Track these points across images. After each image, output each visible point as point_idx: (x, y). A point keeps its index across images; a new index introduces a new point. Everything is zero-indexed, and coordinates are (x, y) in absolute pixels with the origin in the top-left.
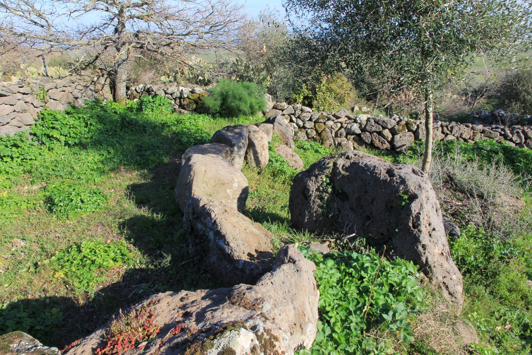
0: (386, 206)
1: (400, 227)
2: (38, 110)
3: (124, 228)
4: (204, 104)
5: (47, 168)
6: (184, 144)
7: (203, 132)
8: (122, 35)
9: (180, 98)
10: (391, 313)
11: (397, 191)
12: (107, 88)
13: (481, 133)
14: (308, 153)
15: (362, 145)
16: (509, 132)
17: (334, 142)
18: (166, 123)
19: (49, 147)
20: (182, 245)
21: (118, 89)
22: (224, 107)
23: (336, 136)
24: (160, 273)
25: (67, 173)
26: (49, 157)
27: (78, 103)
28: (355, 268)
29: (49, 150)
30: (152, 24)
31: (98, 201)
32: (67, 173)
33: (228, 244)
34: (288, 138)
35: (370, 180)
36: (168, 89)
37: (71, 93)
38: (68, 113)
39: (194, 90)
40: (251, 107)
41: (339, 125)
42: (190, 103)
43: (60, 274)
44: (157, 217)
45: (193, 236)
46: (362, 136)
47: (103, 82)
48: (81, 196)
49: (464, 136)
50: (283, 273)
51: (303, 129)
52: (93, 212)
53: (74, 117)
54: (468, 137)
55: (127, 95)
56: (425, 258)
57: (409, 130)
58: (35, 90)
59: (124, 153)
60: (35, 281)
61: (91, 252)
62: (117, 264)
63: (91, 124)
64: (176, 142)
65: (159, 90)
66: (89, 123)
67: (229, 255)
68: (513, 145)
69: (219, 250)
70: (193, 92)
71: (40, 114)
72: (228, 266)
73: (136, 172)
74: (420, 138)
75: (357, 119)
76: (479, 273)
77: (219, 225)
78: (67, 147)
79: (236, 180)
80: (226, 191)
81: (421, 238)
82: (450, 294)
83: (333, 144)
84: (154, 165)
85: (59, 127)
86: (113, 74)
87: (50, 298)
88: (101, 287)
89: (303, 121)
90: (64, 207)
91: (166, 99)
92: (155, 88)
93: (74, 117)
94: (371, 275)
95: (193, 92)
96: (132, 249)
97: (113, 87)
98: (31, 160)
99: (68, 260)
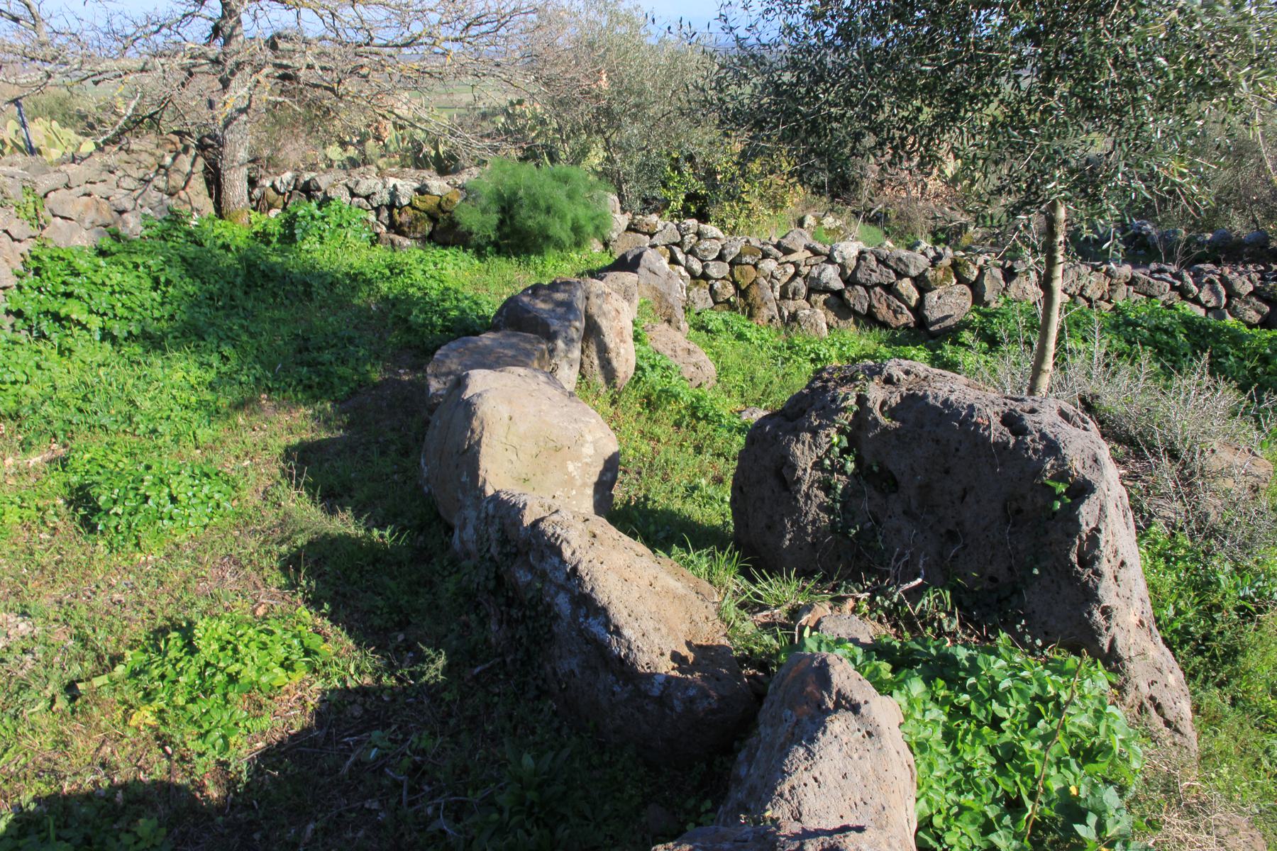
0: (1005, 508)
1: (1043, 564)
2: (23, 248)
3: (298, 571)
4: (458, 224)
5: (64, 404)
6: (427, 334)
7: (460, 296)
8: (234, 45)
9: (391, 206)
10: (1092, 819)
11: (1038, 471)
12: (198, 184)
13: (1127, 284)
14: (720, 342)
15: (846, 318)
16: (1190, 280)
17: (780, 310)
18: (362, 273)
19: (60, 346)
20: (464, 618)
21: (226, 187)
22: (507, 230)
23: (784, 295)
24: (416, 697)
25: (119, 418)
26: (64, 374)
27: (125, 223)
28: (973, 690)
29: (61, 353)
30: (306, 14)
31: (217, 496)
32: (119, 418)
33: (617, 632)
34: (672, 307)
35: (960, 442)
36: (357, 183)
37: (108, 199)
38: (102, 253)
39: (426, 186)
40: (576, 229)
41: (791, 270)
42: (417, 219)
43: (145, 716)
44: (382, 536)
45: (502, 600)
46: (847, 295)
47: (188, 168)
48: (169, 486)
49: (1088, 293)
50: (835, 747)
51: (702, 281)
52: (205, 527)
53: (122, 264)
54: (1099, 294)
55: (251, 200)
56: (1109, 638)
57: (961, 280)
58: (11, 194)
59: (263, 358)
60: (78, 742)
61: (223, 649)
62: (296, 678)
63: (168, 282)
64: (394, 324)
65: (334, 186)
66: (162, 279)
67: (622, 661)
68: (1201, 312)
69: (587, 643)
70: (422, 190)
71: (29, 259)
72: (617, 689)
73: (303, 410)
74: (986, 299)
75: (835, 254)
76: (1206, 649)
77: (587, 578)
78: (107, 345)
79: (589, 438)
80: (564, 467)
81: (1100, 592)
82: (1168, 723)
83: (777, 317)
84: (346, 389)
85: (83, 292)
86: (211, 146)
87: (124, 787)
88: (260, 745)
89: (702, 261)
90: (126, 516)
91: (354, 209)
92: (324, 181)
93: (122, 264)
94: (1017, 711)
95: (422, 190)
96: (328, 630)
97: (214, 181)
98: (14, 383)
99: (163, 677)
